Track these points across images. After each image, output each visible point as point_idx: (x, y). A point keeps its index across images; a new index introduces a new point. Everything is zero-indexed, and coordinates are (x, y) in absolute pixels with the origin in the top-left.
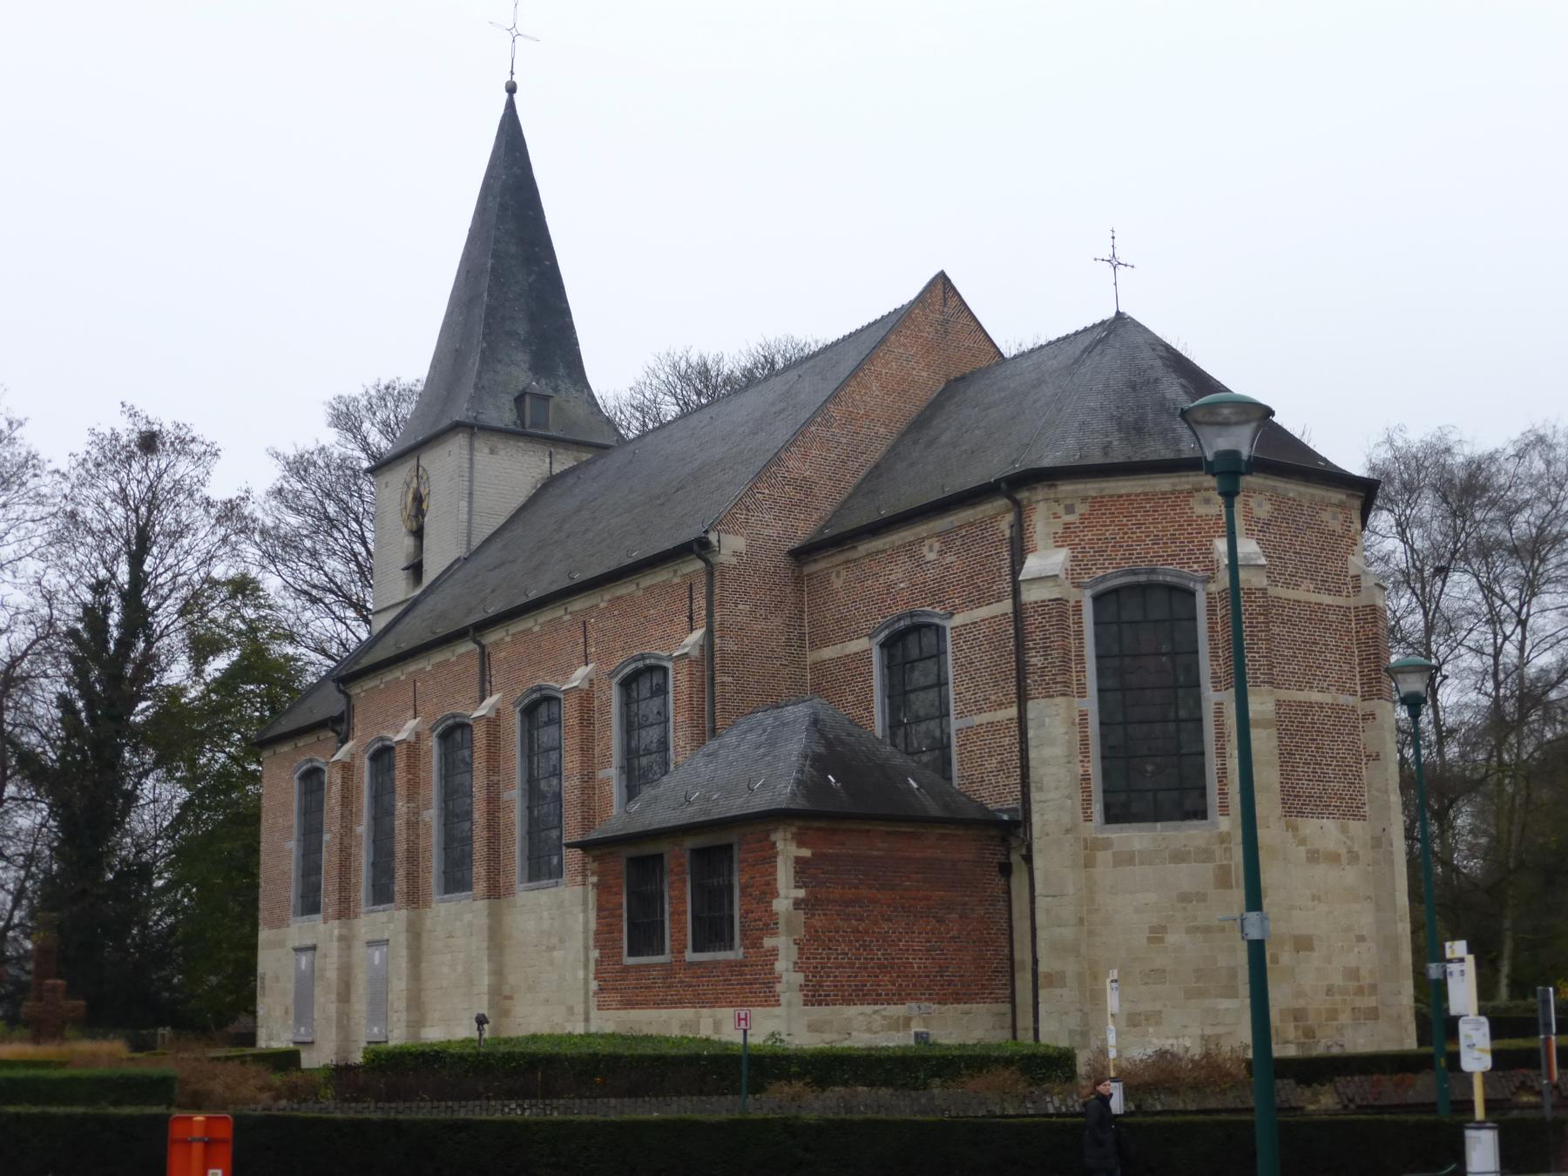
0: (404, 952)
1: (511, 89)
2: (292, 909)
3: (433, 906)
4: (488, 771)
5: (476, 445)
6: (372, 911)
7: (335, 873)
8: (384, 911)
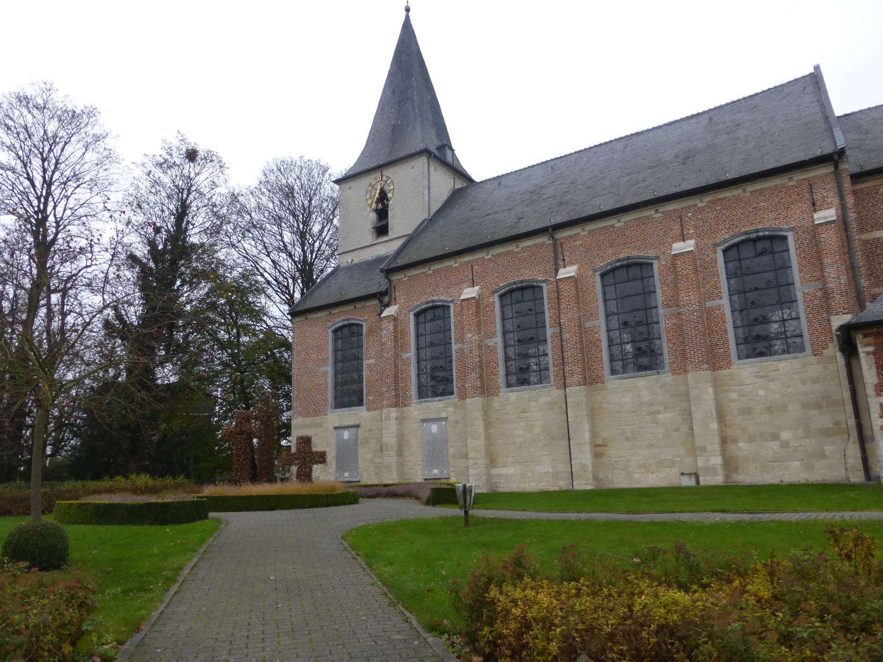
1: (408, 10)
8: (439, 400)
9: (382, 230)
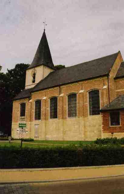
1: (45, 30)
9: (34, 81)
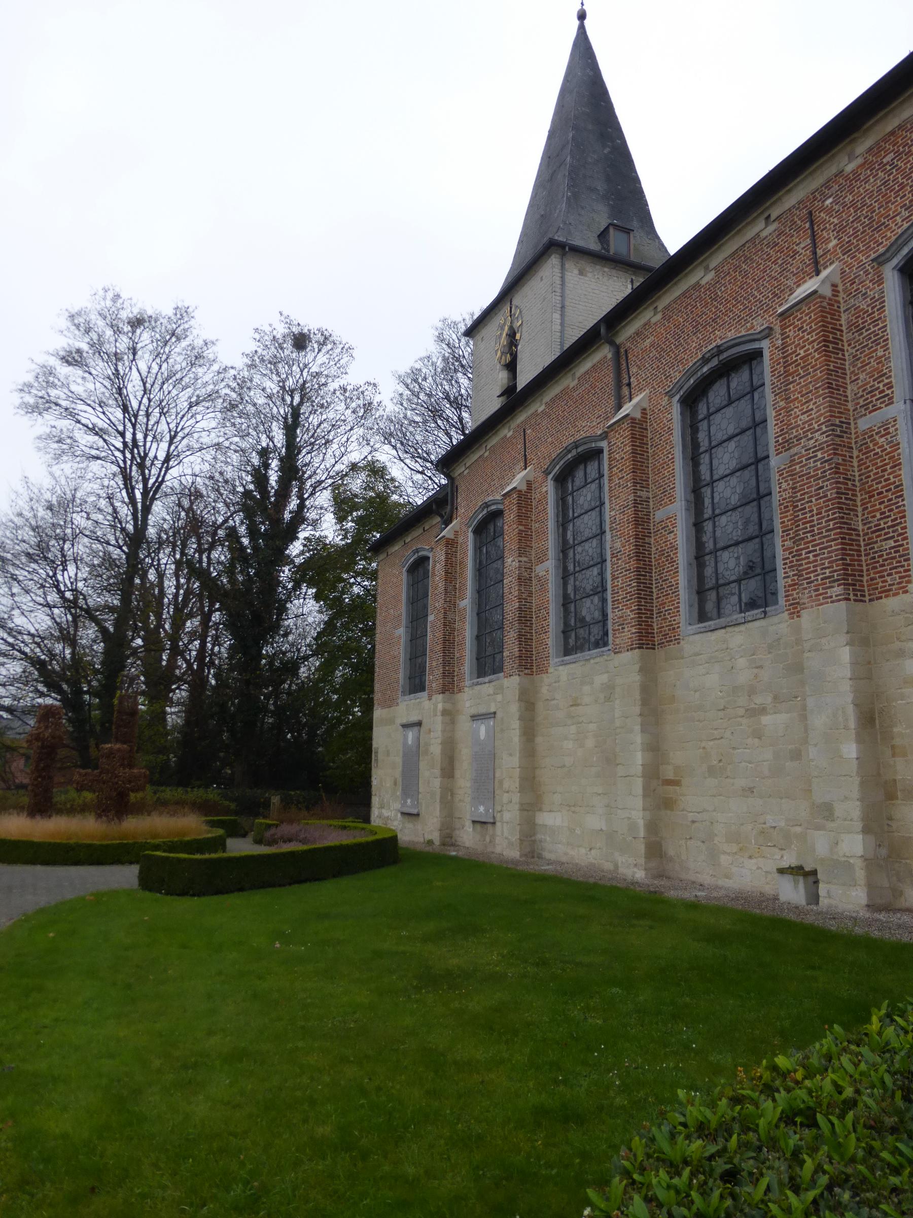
0: (516, 724)
1: (582, 16)
2: (401, 689)
3: (551, 670)
4: (635, 484)
5: (567, 266)
6: (478, 684)
7: (439, 647)
8: (490, 682)
